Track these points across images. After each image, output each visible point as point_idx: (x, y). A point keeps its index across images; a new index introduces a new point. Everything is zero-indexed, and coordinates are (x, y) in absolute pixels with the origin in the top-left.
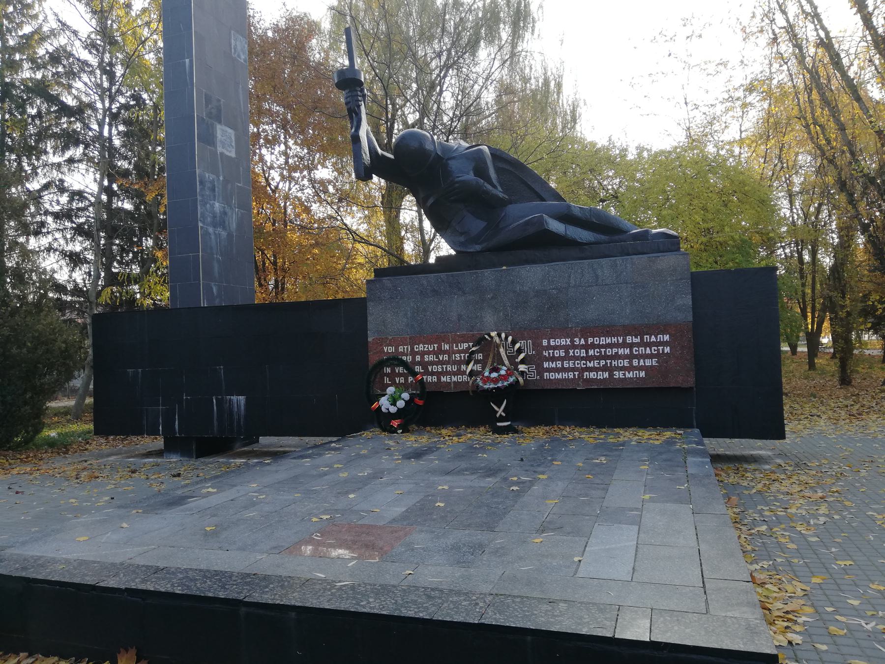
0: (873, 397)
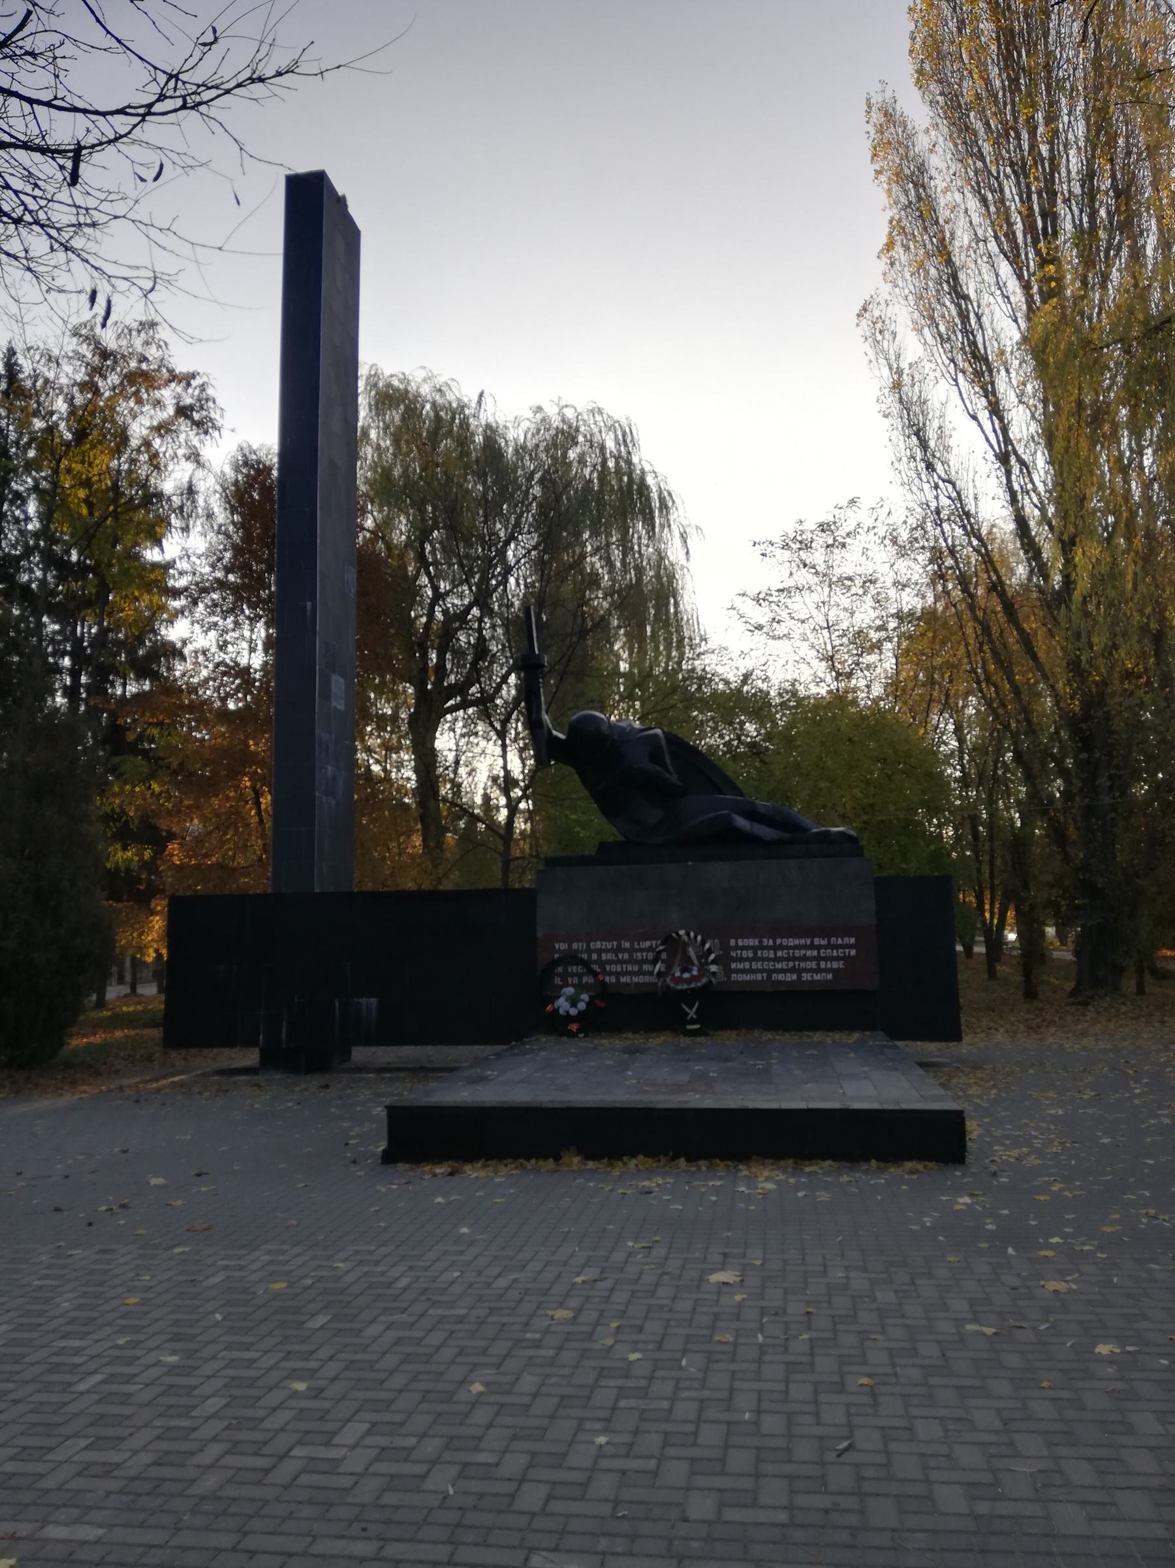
0: (1057, 1011)
